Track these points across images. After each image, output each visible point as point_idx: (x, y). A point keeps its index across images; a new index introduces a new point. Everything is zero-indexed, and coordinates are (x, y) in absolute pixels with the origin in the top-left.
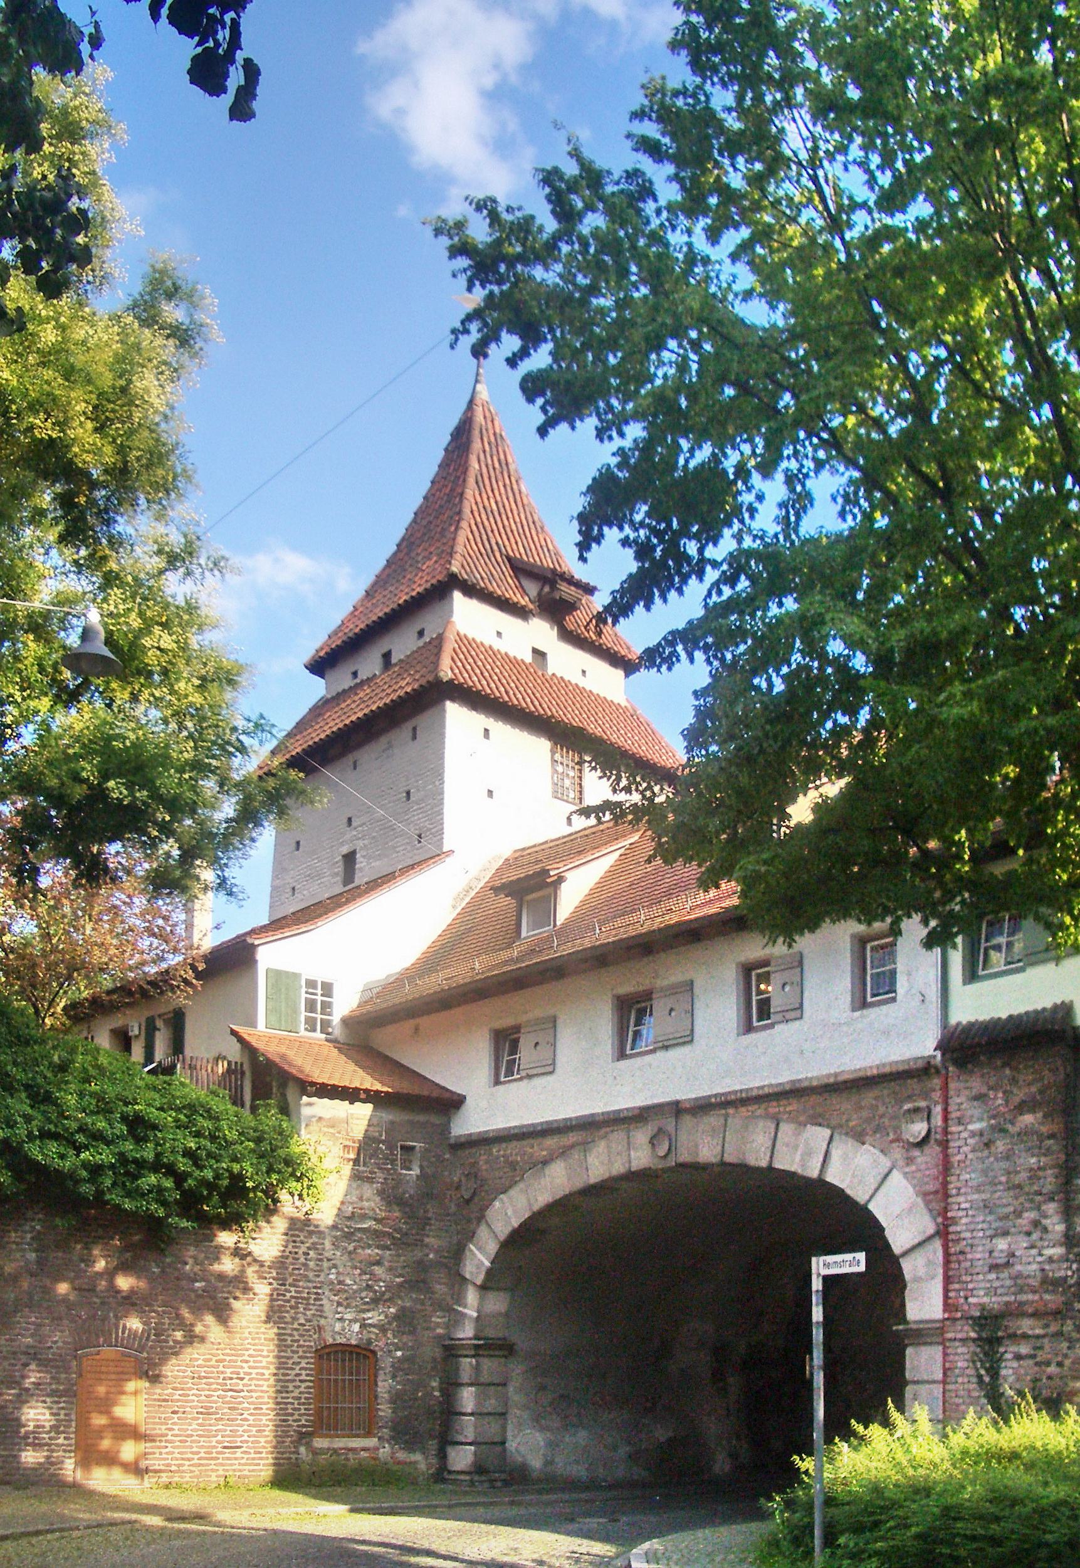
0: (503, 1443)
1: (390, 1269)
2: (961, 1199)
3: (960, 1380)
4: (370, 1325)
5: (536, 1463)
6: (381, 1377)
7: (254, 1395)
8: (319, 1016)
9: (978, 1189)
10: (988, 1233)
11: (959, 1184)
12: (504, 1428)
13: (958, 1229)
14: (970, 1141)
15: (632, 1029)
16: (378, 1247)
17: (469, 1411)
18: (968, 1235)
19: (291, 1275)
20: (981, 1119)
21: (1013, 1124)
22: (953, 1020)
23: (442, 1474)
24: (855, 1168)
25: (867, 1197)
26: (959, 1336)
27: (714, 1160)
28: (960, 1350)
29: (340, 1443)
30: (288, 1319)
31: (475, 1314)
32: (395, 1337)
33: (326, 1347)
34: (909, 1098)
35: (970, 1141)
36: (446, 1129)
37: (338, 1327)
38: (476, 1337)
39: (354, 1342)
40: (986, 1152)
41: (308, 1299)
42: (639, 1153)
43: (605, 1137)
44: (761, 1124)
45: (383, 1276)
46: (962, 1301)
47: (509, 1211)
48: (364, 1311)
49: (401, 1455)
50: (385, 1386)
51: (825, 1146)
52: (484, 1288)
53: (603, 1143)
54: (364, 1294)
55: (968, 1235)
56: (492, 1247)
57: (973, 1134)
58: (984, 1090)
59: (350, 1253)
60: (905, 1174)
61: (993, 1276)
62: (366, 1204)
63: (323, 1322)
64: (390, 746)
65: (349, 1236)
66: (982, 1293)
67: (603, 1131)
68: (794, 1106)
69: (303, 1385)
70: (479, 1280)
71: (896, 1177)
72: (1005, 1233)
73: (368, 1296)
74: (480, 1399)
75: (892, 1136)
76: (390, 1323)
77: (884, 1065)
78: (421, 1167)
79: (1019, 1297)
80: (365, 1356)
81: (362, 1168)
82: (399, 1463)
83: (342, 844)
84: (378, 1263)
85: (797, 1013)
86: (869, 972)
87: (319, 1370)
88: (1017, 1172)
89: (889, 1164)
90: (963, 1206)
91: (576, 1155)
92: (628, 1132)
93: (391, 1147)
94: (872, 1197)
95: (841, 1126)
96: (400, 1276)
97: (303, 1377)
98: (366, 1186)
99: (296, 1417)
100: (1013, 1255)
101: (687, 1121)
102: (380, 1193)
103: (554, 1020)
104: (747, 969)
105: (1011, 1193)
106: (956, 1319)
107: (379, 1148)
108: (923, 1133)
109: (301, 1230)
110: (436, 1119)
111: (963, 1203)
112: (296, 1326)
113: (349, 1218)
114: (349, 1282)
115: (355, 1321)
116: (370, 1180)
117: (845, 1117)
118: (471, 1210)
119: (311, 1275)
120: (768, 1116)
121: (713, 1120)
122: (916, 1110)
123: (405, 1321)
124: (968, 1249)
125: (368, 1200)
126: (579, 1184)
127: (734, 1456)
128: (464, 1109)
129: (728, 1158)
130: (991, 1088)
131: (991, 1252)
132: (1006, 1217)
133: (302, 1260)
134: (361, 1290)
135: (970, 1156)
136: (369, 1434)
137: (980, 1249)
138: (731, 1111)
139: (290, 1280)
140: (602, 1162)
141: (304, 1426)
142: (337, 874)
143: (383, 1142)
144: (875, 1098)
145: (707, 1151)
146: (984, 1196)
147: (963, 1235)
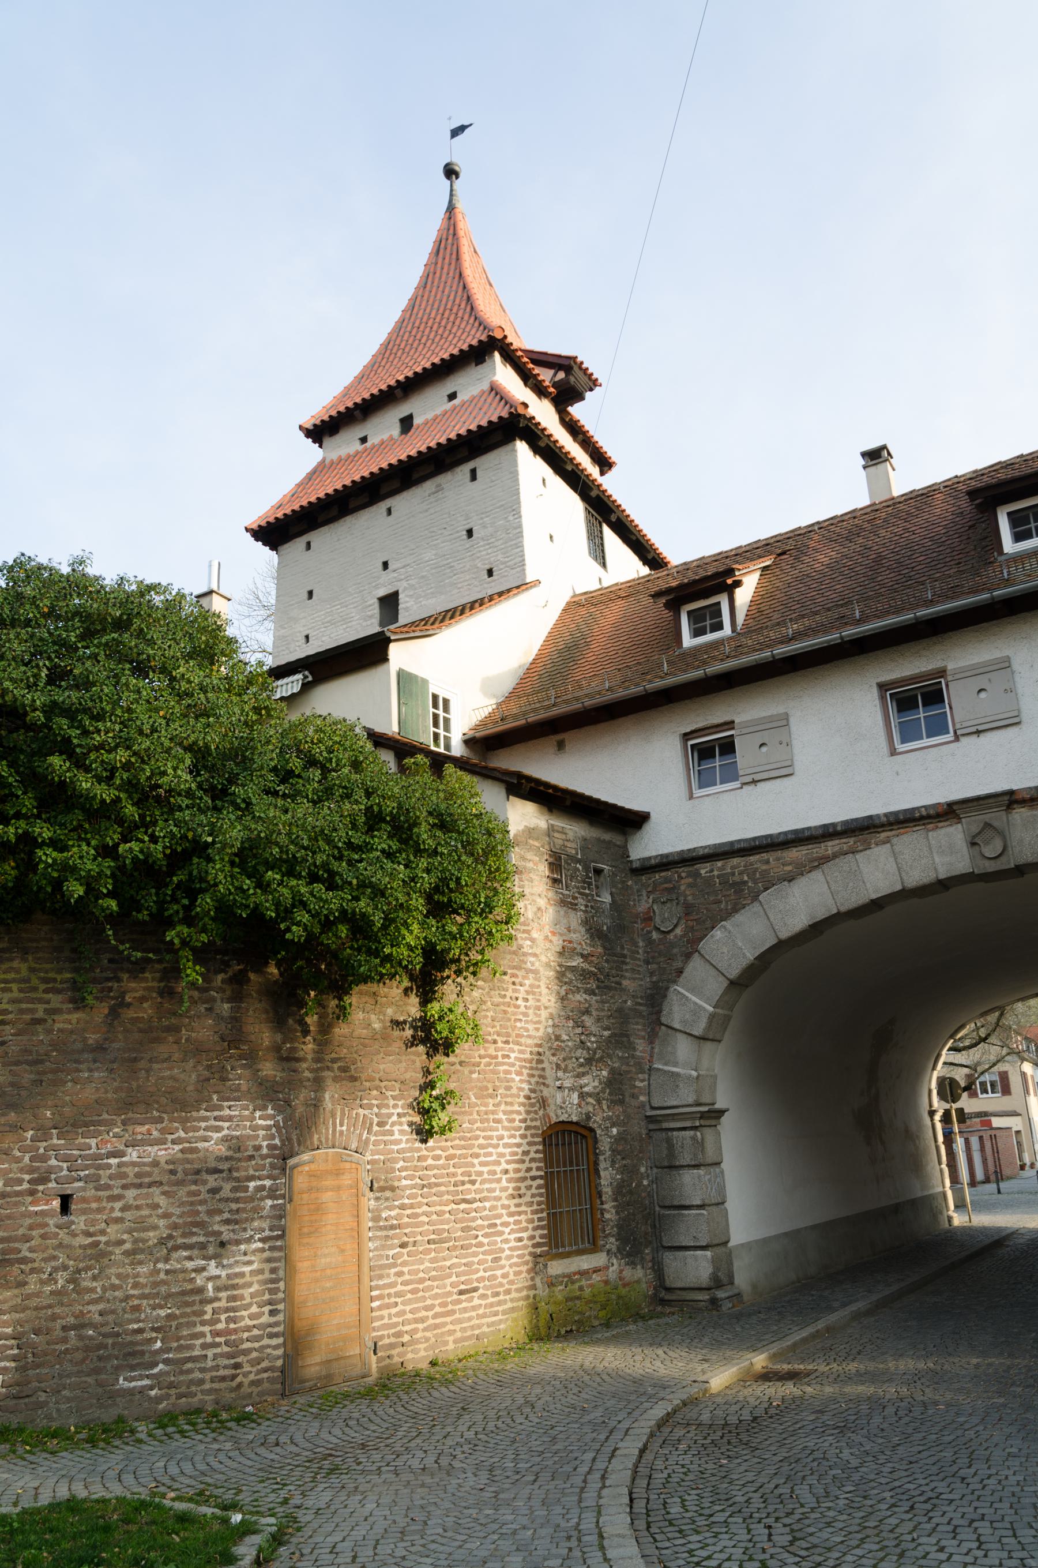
6: (602, 1165)
7: (487, 1204)
8: (708, 623)
25: (721, 978)
39: (575, 1119)
42: (944, 853)
43: (887, 841)
47: (738, 940)
48: (580, 1076)
49: (628, 1273)
56: (716, 987)
64: (439, 488)
67: (883, 835)
76: (603, 1091)
80: (584, 1137)
83: (377, 587)
84: (587, 1012)
93: (586, 868)
96: (607, 1029)
98: (572, 913)
101: (1020, 814)
102: (585, 922)
103: (786, 717)
110: (617, 839)
123: (616, 1087)
136: (594, 1248)
140: (878, 872)
142: (371, 617)
143: (579, 861)
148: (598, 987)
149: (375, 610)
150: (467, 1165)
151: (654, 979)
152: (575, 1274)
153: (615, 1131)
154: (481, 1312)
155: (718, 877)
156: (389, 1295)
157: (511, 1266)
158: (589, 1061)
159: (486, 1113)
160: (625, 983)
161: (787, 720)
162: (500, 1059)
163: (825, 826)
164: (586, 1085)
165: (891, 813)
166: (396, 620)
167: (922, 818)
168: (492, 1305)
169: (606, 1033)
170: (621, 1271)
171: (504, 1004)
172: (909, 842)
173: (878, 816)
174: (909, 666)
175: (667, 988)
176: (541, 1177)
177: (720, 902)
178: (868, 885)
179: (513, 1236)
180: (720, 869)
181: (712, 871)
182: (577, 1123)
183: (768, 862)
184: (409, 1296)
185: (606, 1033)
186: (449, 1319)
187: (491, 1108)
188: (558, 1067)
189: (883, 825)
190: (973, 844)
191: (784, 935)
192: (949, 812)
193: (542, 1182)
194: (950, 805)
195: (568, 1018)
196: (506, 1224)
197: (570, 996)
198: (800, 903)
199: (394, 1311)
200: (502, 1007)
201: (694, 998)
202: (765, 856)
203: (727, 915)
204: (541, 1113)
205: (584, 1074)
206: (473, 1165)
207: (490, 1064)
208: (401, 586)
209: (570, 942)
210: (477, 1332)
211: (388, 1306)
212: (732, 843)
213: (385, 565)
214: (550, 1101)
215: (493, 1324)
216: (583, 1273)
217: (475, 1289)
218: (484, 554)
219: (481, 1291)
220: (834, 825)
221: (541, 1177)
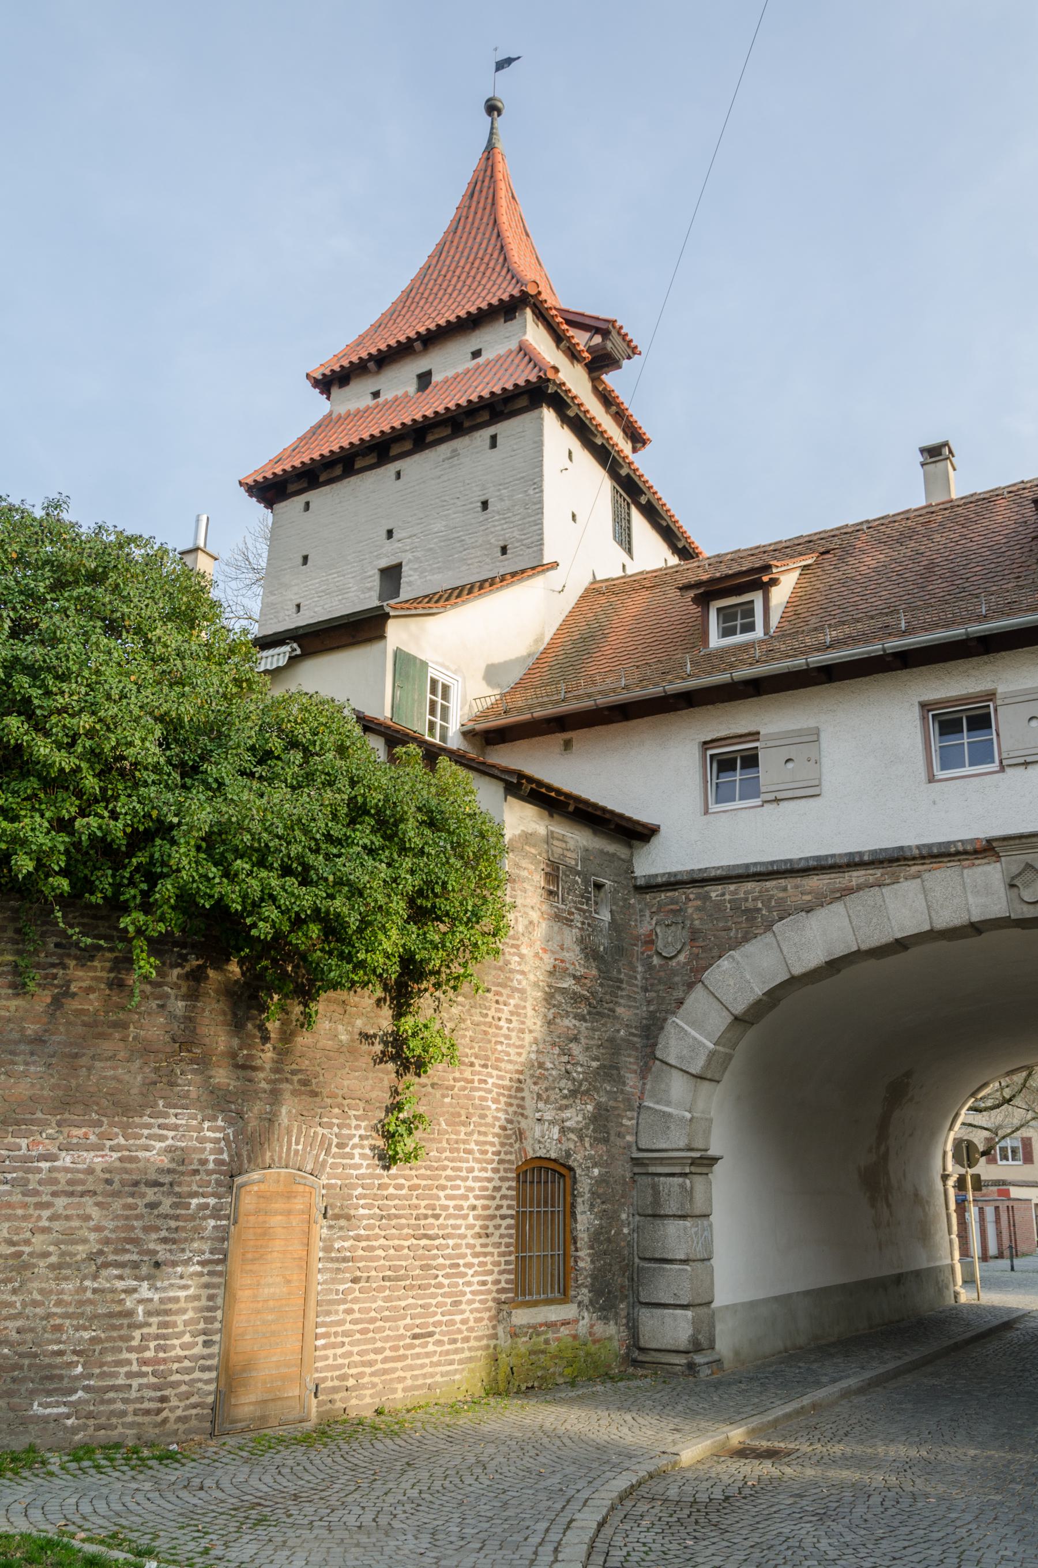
4: (571, 1130)
6: (580, 1209)
8: (739, 622)
16: (576, 1016)
25: (725, 1013)
39: (553, 1155)
43: (917, 876)
47: (746, 973)
48: (562, 1108)
49: (599, 1328)
56: (719, 1021)
62: (566, 955)
67: (914, 869)
73: (566, 1085)
76: (587, 1127)
83: (378, 557)
84: (575, 1039)
96: (596, 1059)
98: (566, 930)
102: (581, 941)
114: (549, 1065)
115: (552, 1123)
116: (569, 922)
123: (601, 1123)
125: (568, 950)
128: (655, 841)
140: (906, 908)
142: (370, 589)
143: (578, 873)
148: (589, 1013)
149: (375, 582)
151: (652, 1008)
152: (541, 1325)
153: (596, 1171)
154: (435, 1359)
156: (336, 1334)
157: (471, 1311)
158: (574, 1093)
160: (619, 1010)
161: (818, 735)
162: (476, 1084)
164: (569, 1119)
165: (924, 845)
167: (958, 853)
168: (447, 1353)
169: (595, 1064)
170: (592, 1326)
171: (485, 1024)
172: (942, 879)
175: (665, 1020)
177: (730, 929)
178: (893, 923)
180: (732, 893)
181: (723, 894)
183: (785, 889)
184: (358, 1336)
185: (595, 1064)
186: (399, 1365)
187: (462, 1136)
191: (797, 970)
193: (512, 1222)
195: (554, 1044)
196: (469, 1265)
198: (816, 937)
201: (694, 1033)
203: (737, 944)
204: (517, 1146)
205: (567, 1107)
206: (438, 1198)
208: (405, 558)
209: (562, 961)
210: (429, 1381)
213: (390, 534)
216: (550, 1325)
219: (437, 1337)
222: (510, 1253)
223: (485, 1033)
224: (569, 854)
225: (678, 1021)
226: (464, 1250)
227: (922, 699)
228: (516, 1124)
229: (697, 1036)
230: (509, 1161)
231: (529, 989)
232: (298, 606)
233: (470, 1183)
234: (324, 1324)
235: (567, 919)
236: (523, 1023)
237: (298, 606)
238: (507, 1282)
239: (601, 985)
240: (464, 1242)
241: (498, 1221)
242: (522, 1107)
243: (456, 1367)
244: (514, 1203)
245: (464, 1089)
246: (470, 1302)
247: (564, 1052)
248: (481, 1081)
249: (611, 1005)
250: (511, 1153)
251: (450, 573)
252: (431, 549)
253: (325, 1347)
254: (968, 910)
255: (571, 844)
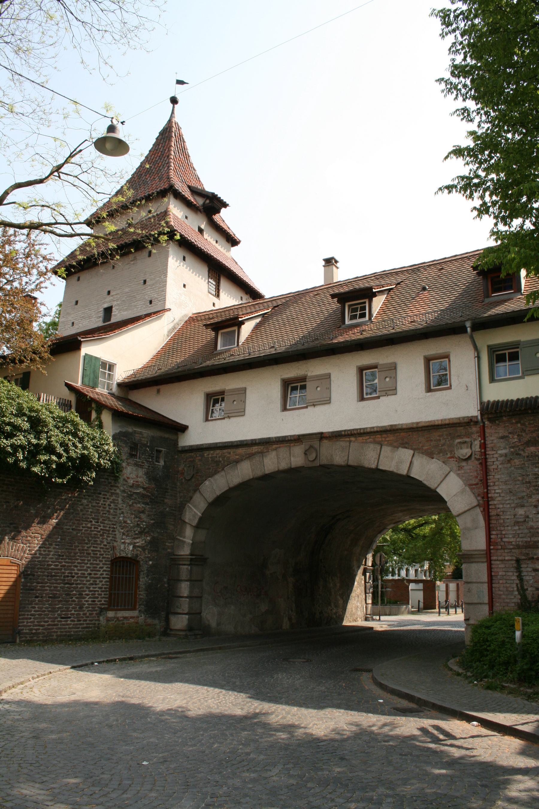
0: (200, 613)
1: (149, 516)
2: (496, 488)
3: (501, 582)
4: (139, 547)
5: (213, 624)
6: (141, 576)
7: (79, 586)
9: (505, 483)
10: (513, 505)
11: (494, 480)
12: (201, 606)
13: (495, 502)
14: (499, 459)
15: (211, 408)
16: (143, 503)
17: (186, 595)
18: (501, 506)
19: (102, 517)
20: (505, 448)
21: (523, 450)
22: (485, 399)
23: (167, 631)
24: (426, 469)
25: (436, 485)
26: (500, 558)
27: (343, 464)
28: (500, 566)
29: (121, 614)
30: (99, 542)
31: (191, 542)
32: (149, 553)
33: (116, 558)
34: (459, 437)
35: (499, 459)
36: (176, 442)
37: (122, 547)
38: (191, 554)
39: (129, 556)
40: (509, 465)
41: (109, 531)
42: (296, 458)
43: (276, 449)
44: (372, 446)
45: (145, 519)
46: (499, 540)
47: (216, 485)
48: (135, 538)
49: (149, 621)
50: (143, 580)
51: (410, 459)
52: (197, 527)
53: (274, 453)
54: (135, 529)
55: (501, 506)
56: (203, 506)
57: (501, 455)
58: (506, 434)
59: (130, 506)
60: (458, 475)
61: (517, 528)
62: (139, 479)
63: (115, 544)
65: (130, 496)
66: (511, 536)
67: (274, 446)
68: (391, 437)
69: (104, 580)
70: (195, 523)
71: (452, 475)
72: (522, 506)
74: (192, 588)
75: (449, 455)
76: (147, 546)
77: (445, 420)
78: (165, 462)
79: (532, 539)
81: (138, 460)
82: (150, 625)
83: (104, 303)
84: (143, 512)
85: (329, 402)
86: (431, 375)
87: (112, 571)
88: (528, 475)
89: (449, 469)
90: (497, 491)
91: (257, 458)
92: (290, 447)
94: (439, 485)
95: (418, 449)
97: (104, 576)
99: (99, 599)
100: (528, 517)
101: (325, 443)
102: (146, 474)
104: (361, 370)
105: (525, 485)
106: (498, 549)
107: (146, 450)
108: (469, 454)
109: (108, 492)
110: (172, 437)
111: (498, 491)
112: (102, 546)
113: (131, 487)
114: (129, 522)
116: (141, 467)
117: (421, 445)
118: (194, 484)
119: (111, 517)
120: (375, 442)
121: (342, 443)
122: (465, 442)
124: (501, 513)
126: (259, 473)
127: (290, 619)
129: (351, 463)
130: (510, 433)
131: (515, 515)
132: (523, 498)
133: (107, 509)
134: (134, 527)
135: (500, 466)
136: (134, 609)
137: (508, 513)
138: (353, 439)
139: (101, 520)
140: (271, 463)
141: (103, 604)
142: (100, 317)
143: (148, 447)
144: (439, 436)
145: (339, 459)
146: (509, 487)
147: (497, 506)
148: (151, 502)
149: (101, 314)
150: (72, 570)
151: (181, 500)
152: (121, 617)
153: (151, 563)
154: (71, 626)
155: (211, 458)
156: (28, 615)
157: (88, 611)
158: (141, 533)
159: (83, 550)
160: (166, 501)
161: (245, 391)
162: (93, 529)
163: (252, 440)
164: (137, 543)
165: (277, 437)
166: (110, 320)
167: (289, 440)
168: (77, 624)
169: (152, 522)
170: (145, 620)
171: (98, 506)
172: (283, 451)
173: (272, 438)
174: (292, 371)
175: (186, 504)
176: (108, 578)
177: (210, 469)
178: (266, 468)
179: (90, 600)
180: (212, 454)
181: (208, 455)
182: (130, 558)
183: (230, 453)
184: (37, 616)
185: (152, 522)
186: (55, 627)
187: (86, 548)
188: (124, 534)
189: (274, 442)
190: (305, 454)
191: (232, 485)
192: (298, 439)
193: (108, 580)
194: (299, 436)
195: (132, 514)
196: (88, 595)
197: (135, 505)
198: (244, 471)
199: (29, 621)
200: (97, 508)
201: (195, 510)
202: (229, 450)
203: (212, 475)
204: (112, 552)
205: (137, 538)
206: (74, 570)
207: (87, 530)
208: (114, 304)
209: (137, 482)
210: (68, 634)
211: (27, 619)
212: (217, 443)
213: (109, 293)
214: (117, 548)
215: (77, 632)
216: (125, 618)
217: (70, 618)
218: (150, 294)
219: (72, 619)
220: (255, 440)
221: (108, 578)
222: (106, 591)
223: (98, 510)
224: (143, 439)
225: (190, 505)
226: (85, 589)
227: (283, 377)
228: (111, 544)
229: (196, 511)
230: (108, 558)
231: (120, 493)
232: (73, 323)
233: (88, 565)
234: (23, 611)
235: (140, 465)
236: (117, 506)
237: (73, 323)
238: (105, 601)
239: (157, 491)
240: (85, 586)
241: (102, 579)
242: (115, 538)
243: (80, 629)
244: (109, 573)
245: (87, 530)
246: (87, 608)
247: (136, 517)
248: (95, 528)
249: (162, 499)
250: (108, 555)
251: (130, 311)
252: (124, 300)
253: (23, 619)
254: (291, 463)
255: (145, 435)
